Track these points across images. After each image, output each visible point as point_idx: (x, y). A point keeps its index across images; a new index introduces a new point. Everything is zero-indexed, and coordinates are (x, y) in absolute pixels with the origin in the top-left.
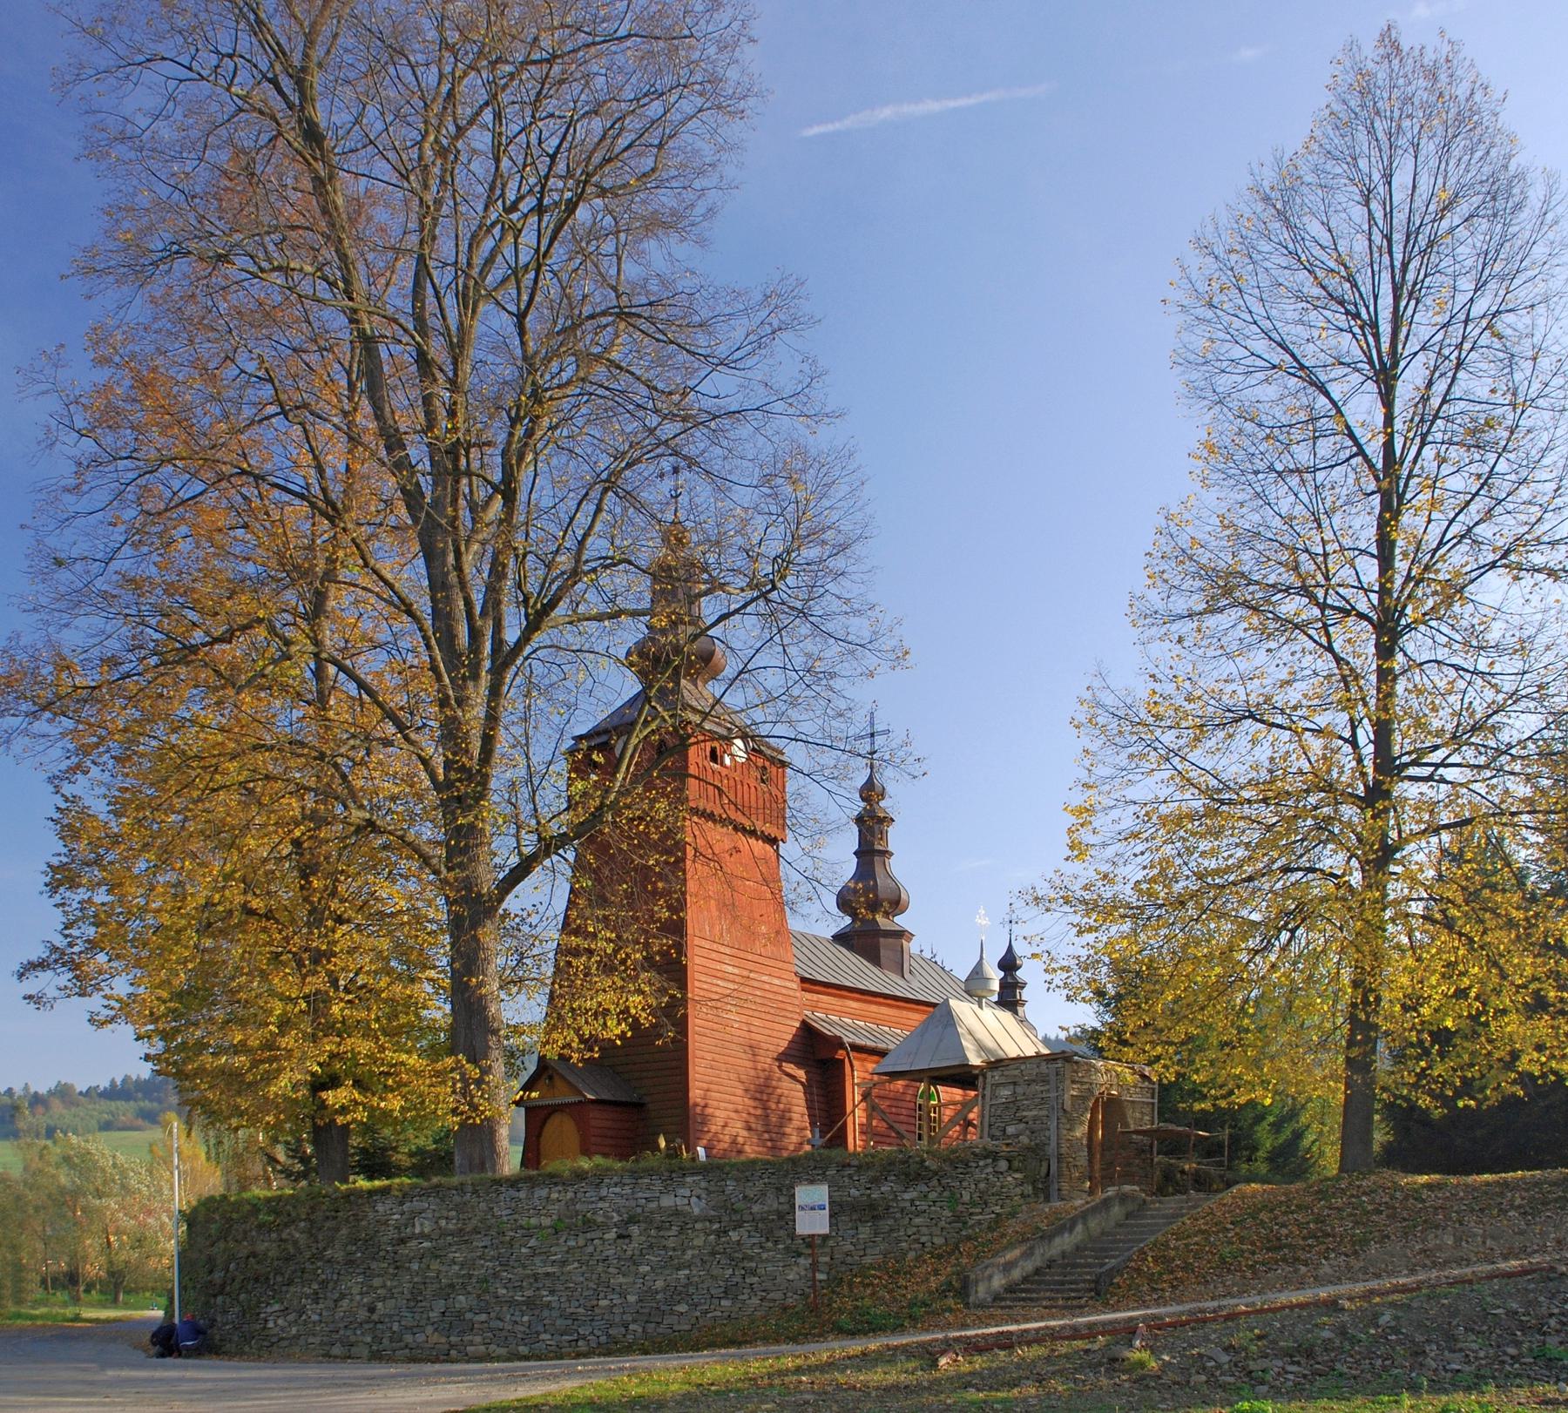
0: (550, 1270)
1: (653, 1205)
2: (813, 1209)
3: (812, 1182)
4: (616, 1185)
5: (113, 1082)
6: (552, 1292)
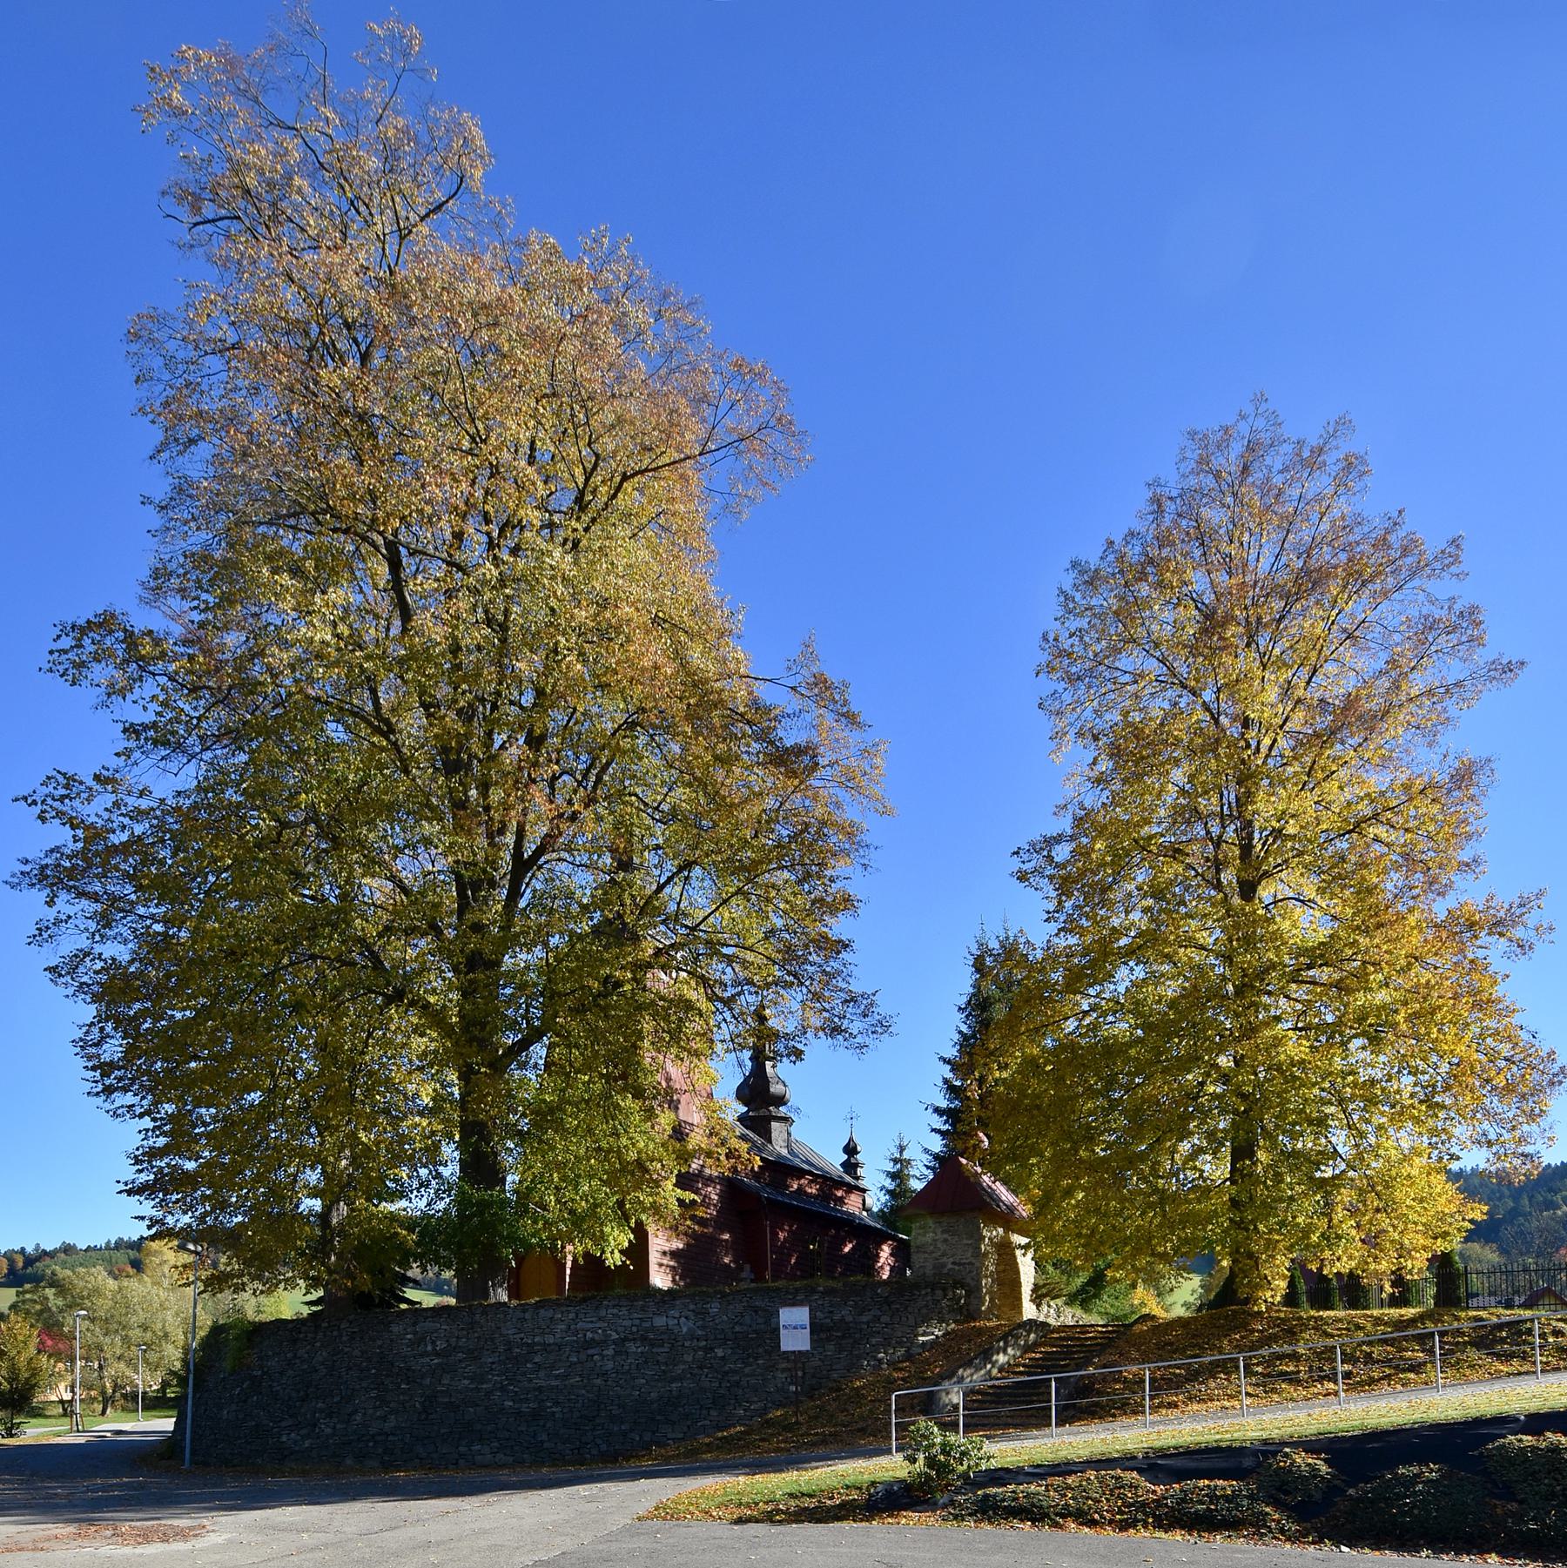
0: (554, 1383)
1: (647, 1325)
2: (795, 1328)
3: (794, 1305)
4: (614, 1306)
5: (109, 1242)
6: (557, 1403)
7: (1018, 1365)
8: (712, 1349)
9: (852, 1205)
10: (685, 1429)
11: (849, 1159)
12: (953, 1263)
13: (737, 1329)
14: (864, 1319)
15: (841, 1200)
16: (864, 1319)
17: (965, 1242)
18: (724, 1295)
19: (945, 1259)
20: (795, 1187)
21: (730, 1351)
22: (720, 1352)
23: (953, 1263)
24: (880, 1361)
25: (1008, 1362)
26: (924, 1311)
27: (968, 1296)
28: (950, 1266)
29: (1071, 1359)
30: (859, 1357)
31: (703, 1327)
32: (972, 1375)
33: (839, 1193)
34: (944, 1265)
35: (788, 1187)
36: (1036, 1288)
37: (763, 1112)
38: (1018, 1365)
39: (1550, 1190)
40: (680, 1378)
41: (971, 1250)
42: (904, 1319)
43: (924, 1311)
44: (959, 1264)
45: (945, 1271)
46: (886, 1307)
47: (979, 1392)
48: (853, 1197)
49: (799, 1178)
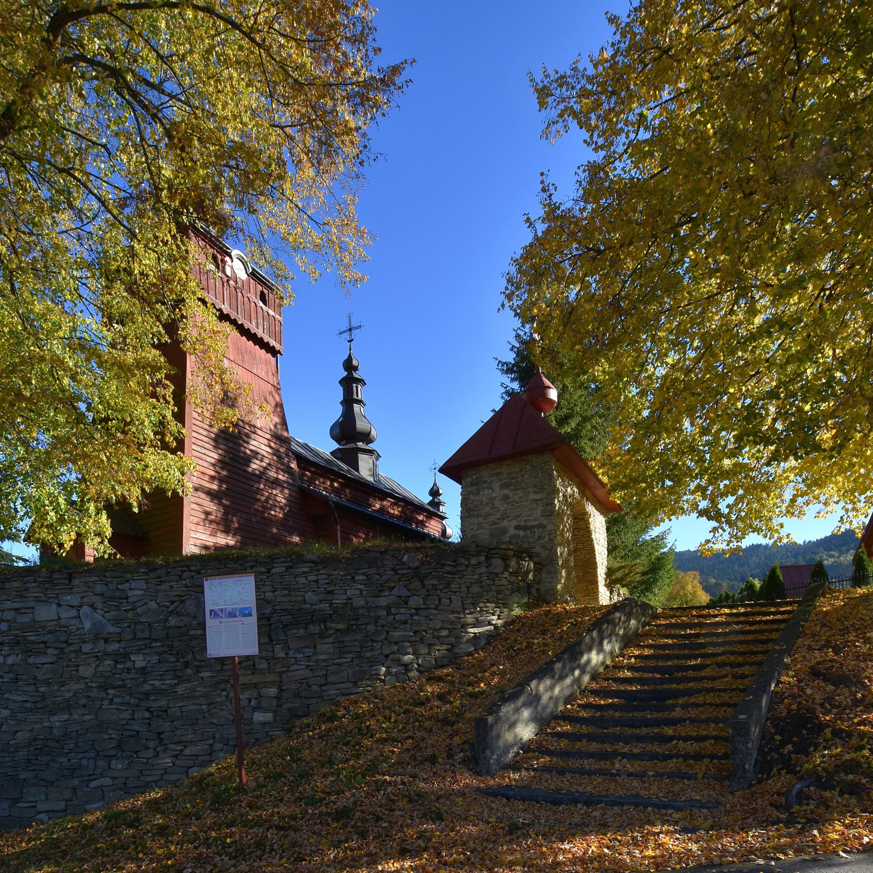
1: (26, 619)
2: (232, 615)
7: (618, 667)
8: (126, 656)
9: (433, 528)
10: (68, 794)
11: (433, 499)
12: (518, 528)
13: (173, 621)
14: (383, 602)
15: (422, 523)
16: (383, 602)
17: (533, 496)
18: (152, 568)
19: (505, 523)
20: (378, 506)
21: (155, 659)
22: (139, 661)
23: (518, 528)
24: (407, 667)
25: (603, 663)
26: (475, 589)
27: (539, 567)
28: (512, 531)
29: (705, 656)
30: (374, 662)
31: (116, 621)
32: (552, 687)
33: (421, 518)
34: (504, 531)
35: (370, 506)
36: (610, 572)
37: (352, 445)
38: (621, 668)
39: (813, 553)
40: (67, 706)
41: (540, 508)
42: (445, 601)
43: (475, 589)
44: (525, 528)
45: (506, 538)
46: (416, 584)
47: (565, 717)
48: (433, 522)
49: (382, 499)
